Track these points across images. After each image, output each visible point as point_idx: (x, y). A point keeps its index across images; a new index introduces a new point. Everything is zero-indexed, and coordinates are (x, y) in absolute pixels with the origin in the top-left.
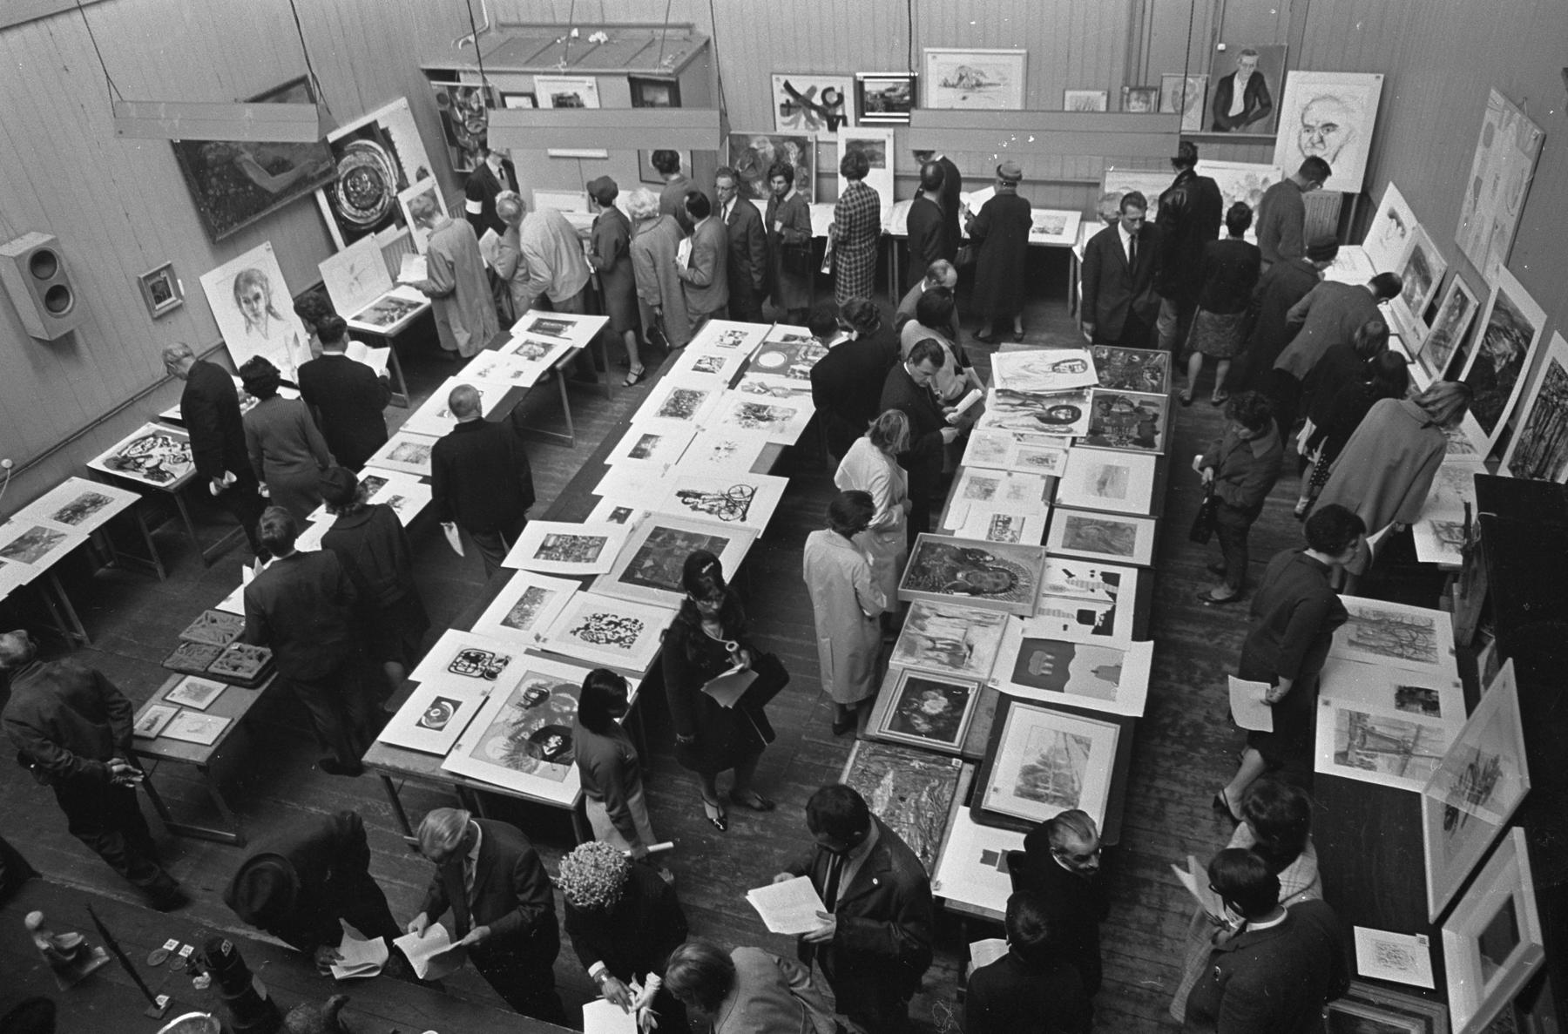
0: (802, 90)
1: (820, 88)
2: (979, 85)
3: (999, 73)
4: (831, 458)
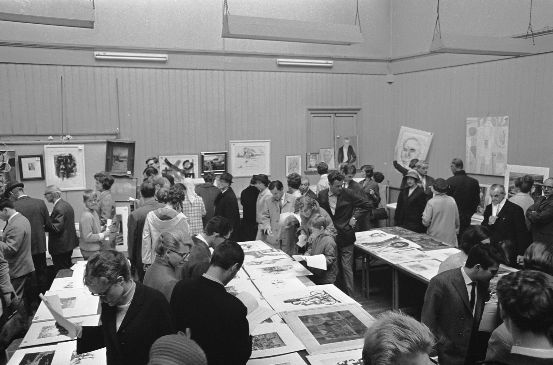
0: (173, 162)
1: (183, 160)
2: (252, 155)
3: (260, 150)
4: (378, 263)
